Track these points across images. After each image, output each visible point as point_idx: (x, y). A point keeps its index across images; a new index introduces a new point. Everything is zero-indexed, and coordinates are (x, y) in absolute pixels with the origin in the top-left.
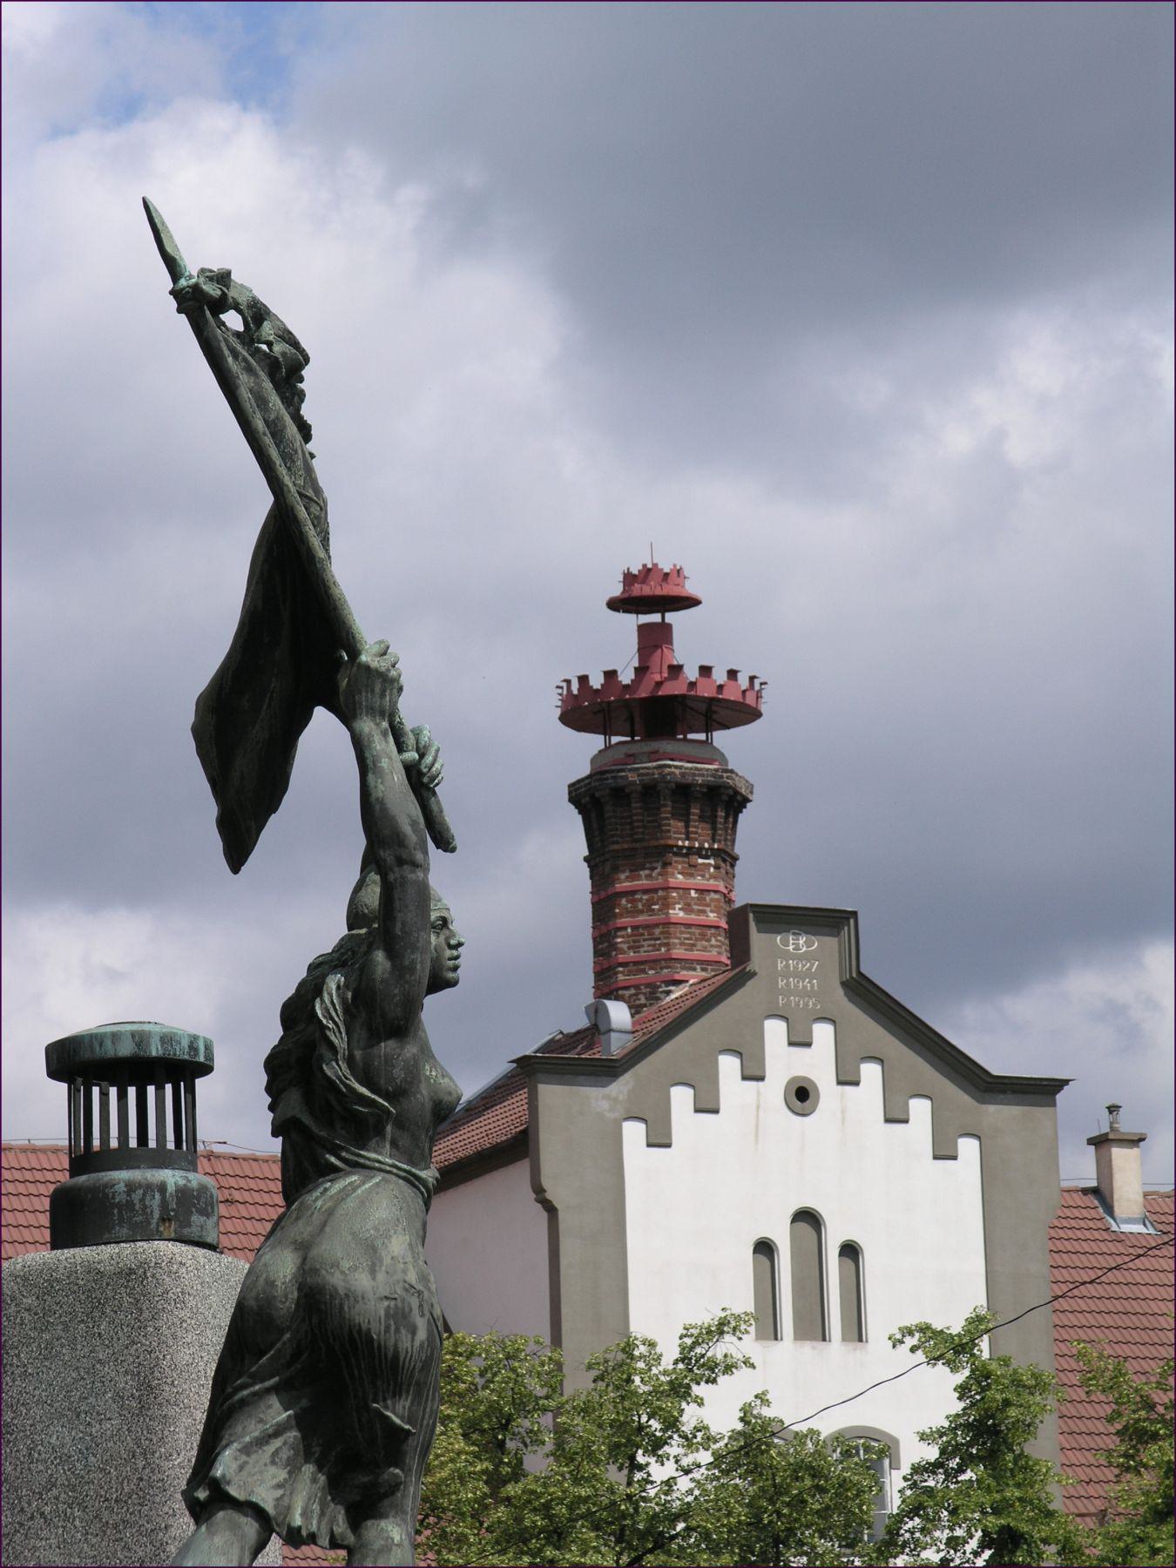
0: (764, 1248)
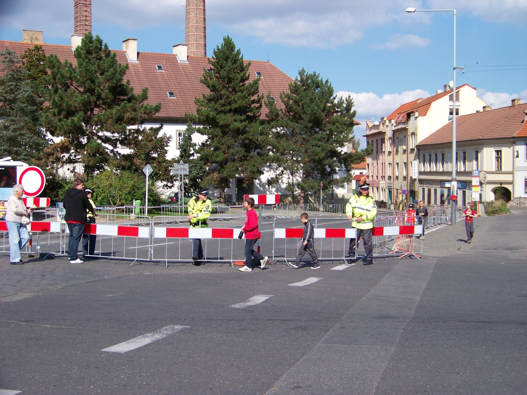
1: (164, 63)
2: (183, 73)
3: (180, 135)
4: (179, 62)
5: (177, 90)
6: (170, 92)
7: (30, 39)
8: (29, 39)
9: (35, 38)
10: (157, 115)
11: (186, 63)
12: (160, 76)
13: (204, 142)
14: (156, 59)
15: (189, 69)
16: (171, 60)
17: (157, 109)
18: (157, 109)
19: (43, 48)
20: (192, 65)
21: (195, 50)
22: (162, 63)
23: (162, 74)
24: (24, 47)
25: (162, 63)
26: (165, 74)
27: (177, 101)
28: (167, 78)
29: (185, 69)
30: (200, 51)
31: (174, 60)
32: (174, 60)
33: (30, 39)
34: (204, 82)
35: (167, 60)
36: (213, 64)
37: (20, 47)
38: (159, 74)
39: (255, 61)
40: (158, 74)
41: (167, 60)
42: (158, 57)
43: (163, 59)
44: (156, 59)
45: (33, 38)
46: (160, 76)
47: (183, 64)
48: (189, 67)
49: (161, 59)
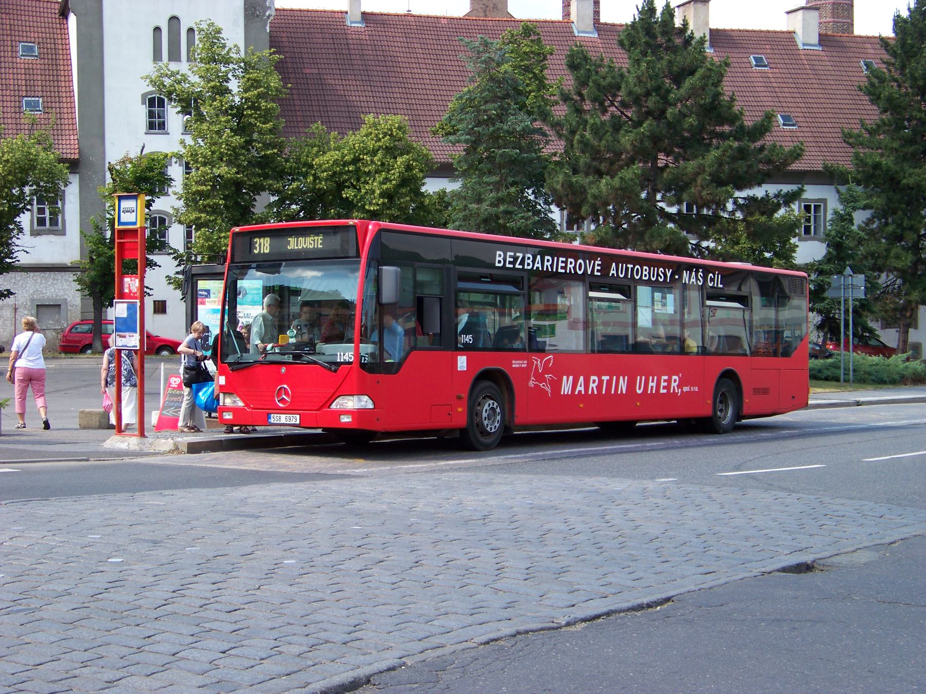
0: (157, 29)
1: (769, 51)
2: (810, 72)
3: (162, 127)
4: (801, 47)
5: (799, 110)
6: (784, 114)
7: (482, 8)
8: (479, 10)
9: (491, 6)
10: (795, 166)
11: (592, 36)
12: (761, 80)
13: (863, 225)
14: (751, 42)
15: (824, 63)
16: (783, 43)
17: (797, 155)
18: (797, 155)
19: (538, 30)
20: (829, 54)
21: (828, 20)
22: (764, 51)
23: (764, 75)
24: (476, 27)
25: (764, 51)
26: (770, 75)
27: (799, 134)
28: (775, 85)
29: (814, 63)
30: (840, 20)
31: (789, 43)
32: (789, 43)
33: (482, 8)
34: (873, 93)
35: (775, 43)
36: (894, 54)
37: (470, 27)
38: (759, 75)
39: (737, 31)
40: (756, 75)
41: (775, 43)
42: (755, 39)
43: (766, 43)
44: (751, 42)
45: (487, 7)
46: (761, 80)
47: (810, 52)
48: (823, 58)
49: (760, 42)
